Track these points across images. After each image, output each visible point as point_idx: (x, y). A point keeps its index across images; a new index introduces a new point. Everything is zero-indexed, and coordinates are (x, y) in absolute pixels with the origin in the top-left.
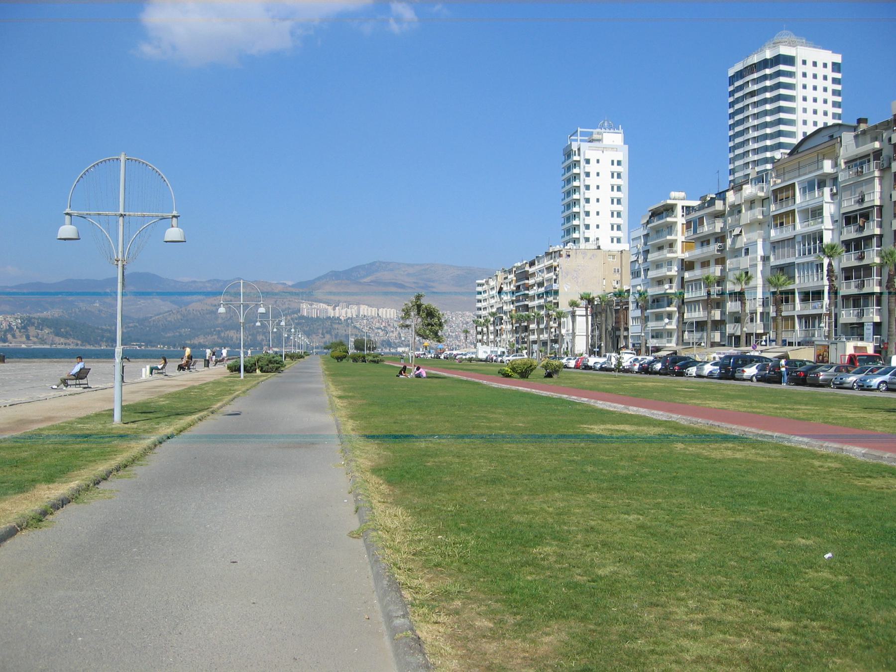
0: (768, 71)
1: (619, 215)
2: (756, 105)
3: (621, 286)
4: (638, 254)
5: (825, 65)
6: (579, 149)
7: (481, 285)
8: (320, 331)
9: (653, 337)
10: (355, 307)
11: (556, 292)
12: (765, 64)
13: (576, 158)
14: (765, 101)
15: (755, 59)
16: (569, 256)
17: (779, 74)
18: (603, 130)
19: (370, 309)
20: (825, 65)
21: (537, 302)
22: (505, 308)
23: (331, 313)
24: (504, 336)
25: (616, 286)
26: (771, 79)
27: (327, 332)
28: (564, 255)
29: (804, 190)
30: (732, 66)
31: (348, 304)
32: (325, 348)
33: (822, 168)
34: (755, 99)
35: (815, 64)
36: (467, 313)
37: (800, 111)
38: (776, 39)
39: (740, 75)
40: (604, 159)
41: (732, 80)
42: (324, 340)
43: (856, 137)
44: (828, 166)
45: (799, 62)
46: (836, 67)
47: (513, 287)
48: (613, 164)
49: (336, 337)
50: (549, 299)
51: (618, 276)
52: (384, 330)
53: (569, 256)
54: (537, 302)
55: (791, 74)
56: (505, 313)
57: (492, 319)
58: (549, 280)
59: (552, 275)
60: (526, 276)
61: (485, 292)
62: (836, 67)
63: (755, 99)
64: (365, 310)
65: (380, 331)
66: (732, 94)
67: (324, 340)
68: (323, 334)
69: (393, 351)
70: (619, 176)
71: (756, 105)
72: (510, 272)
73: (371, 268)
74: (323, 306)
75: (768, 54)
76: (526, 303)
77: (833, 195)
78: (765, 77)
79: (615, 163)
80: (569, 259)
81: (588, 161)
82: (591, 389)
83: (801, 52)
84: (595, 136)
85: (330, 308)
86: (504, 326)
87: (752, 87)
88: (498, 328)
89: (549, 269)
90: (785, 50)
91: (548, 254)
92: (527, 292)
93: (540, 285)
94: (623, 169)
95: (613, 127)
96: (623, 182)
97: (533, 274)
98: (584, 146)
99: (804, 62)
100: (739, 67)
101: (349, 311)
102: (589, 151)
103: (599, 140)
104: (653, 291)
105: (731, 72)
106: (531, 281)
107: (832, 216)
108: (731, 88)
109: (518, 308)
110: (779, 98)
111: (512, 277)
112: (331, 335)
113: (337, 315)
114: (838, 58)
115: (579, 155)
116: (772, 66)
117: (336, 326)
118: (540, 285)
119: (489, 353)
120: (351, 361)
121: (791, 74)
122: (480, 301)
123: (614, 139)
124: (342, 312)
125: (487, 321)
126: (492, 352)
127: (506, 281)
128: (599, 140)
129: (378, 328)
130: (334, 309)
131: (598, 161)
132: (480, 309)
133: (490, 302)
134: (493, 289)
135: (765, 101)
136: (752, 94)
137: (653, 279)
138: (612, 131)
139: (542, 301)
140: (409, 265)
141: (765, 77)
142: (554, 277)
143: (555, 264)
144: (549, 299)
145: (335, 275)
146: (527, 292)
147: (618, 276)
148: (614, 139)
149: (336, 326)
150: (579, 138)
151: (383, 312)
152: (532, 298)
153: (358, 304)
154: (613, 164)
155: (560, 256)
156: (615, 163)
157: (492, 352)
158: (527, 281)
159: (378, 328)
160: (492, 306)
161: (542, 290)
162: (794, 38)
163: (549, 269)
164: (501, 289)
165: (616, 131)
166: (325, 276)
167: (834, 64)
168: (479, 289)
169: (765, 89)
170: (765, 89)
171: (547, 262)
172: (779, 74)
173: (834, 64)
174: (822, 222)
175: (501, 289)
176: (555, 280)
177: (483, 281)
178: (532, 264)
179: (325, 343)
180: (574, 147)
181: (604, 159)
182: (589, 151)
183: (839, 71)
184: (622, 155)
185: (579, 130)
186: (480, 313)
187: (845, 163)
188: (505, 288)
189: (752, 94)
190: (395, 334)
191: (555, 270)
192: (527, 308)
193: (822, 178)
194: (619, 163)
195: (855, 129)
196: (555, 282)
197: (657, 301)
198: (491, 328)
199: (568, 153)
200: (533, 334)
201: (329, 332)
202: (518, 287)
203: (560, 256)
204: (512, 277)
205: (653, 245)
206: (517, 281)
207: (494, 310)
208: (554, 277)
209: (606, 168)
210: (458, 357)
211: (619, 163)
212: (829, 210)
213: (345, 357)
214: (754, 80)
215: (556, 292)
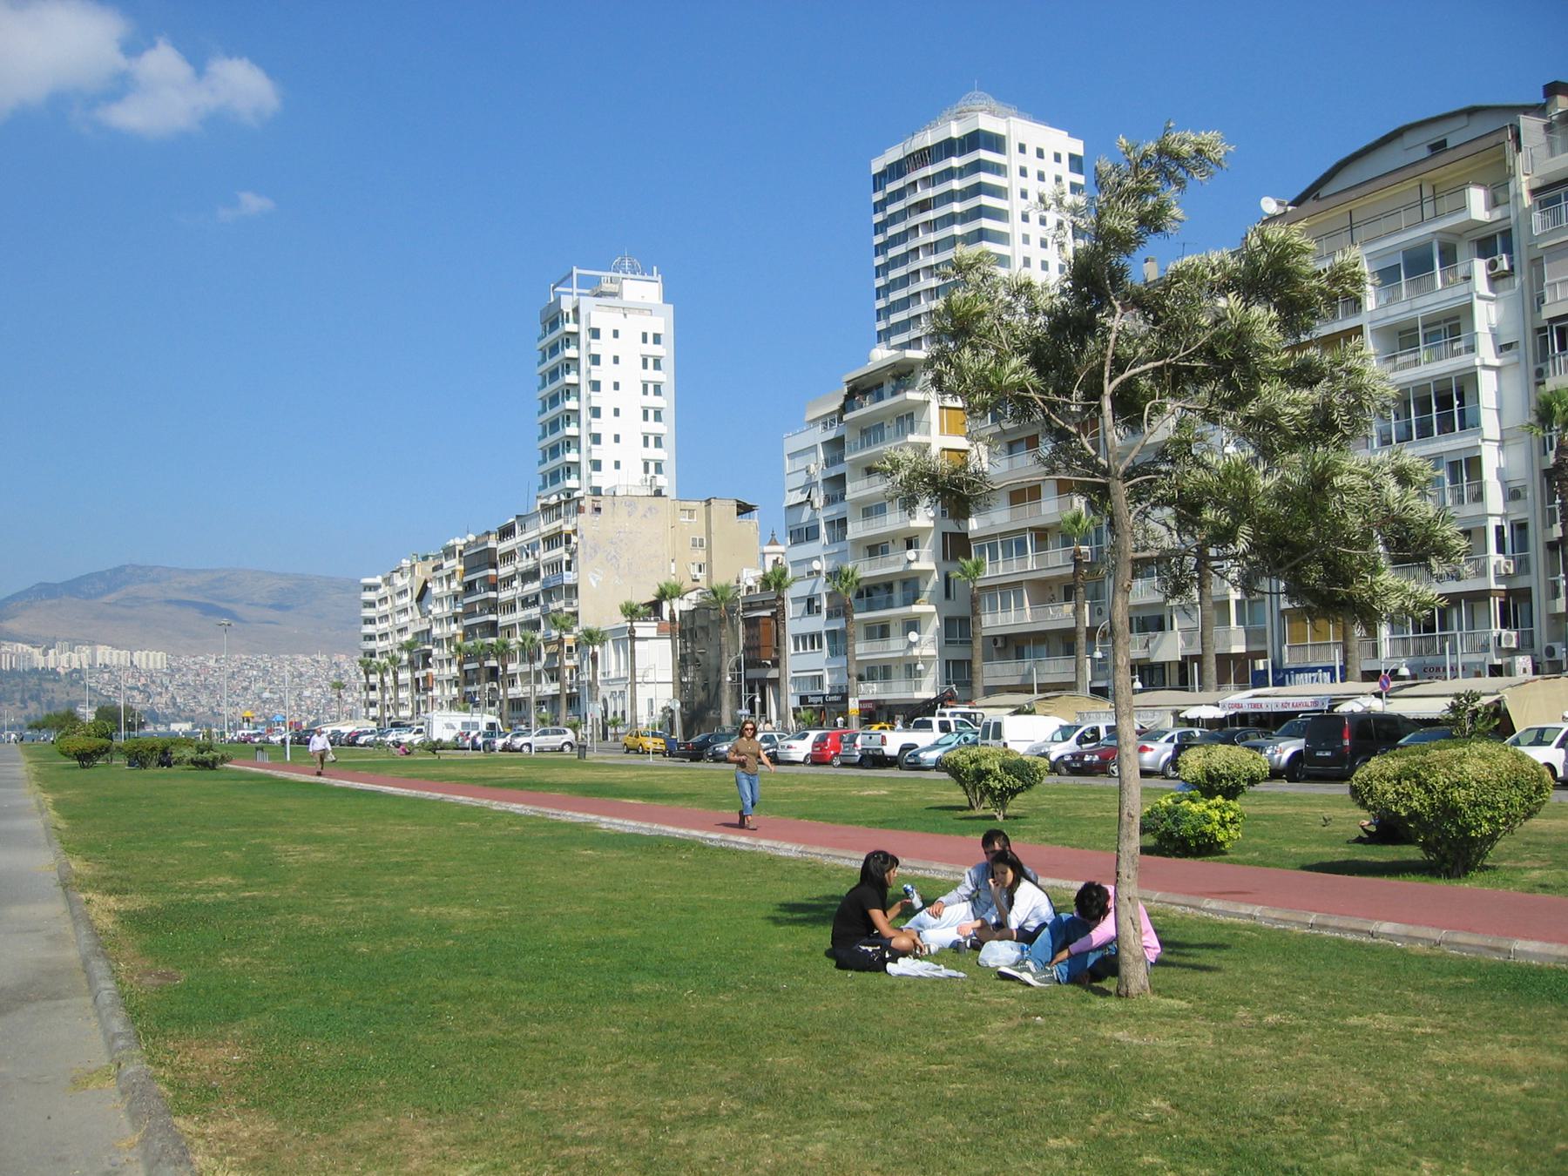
0: (955, 162)
1: (658, 442)
2: (931, 226)
3: (710, 577)
4: (808, 486)
5: (1057, 158)
6: (576, 310)
7: (375, 588)
8: (18, 696)
9: (861, 678)
10: (87, 650)
11: (573, 590)
12: (949, 147)
13: (570, 327)
14: (951, 219)
15: (928, 138)
16: (598, 510)
17: (978, 166)
18: (621, 275)
19: (115, 652)
20: (1057, 158)
21: (520, 615)
22: (436, 631)
23: (39, 660)
24: (436, 692)
25: (699, 576)
26: (961, 177)
27: (31, 698)
28: (589, 509)
29: (1388, 276)
30: (880, 152)
31: (73, 644)
32: (30, 728)
33: (1463, 207)
34: (931, 215)
35: (1040, 153)
36: (301, 658)
37: (1017, 239)
38: (961, 105)
39: (896, 170)
40: (627, 329)
41: (880, 180)
42: (26, 712)
43: (1549, 128)
44: (1477, 205)
45: (1012, 147)
46: (1076, 163)
47: (455, 586)
48: (645, 340)
49: (49, 708)
50: (554, 606)
51: (700, 555)
52: (144, 691)
53: (598, 510)
54: (520, 615)
55: (998, 169)
56: (438, 642)
57: (405, 656)
58: (555, 565)
59: (560, 552)
60: (487, 559)
61: (384, 600)
62: (1076, 163)
63: (931, 215)
64: (105, 654)
65: (135, 693)
66: (880, 206)
67: (26, 712)
68: (23, 701)
69: (162, 729)
70: (657, 366)
71: (931, 226)
72: (449, 552)
73: (114, 579)
74: (22, 647)
75: (956, 130)
76: (492, 617)
77: (1495, 279)
78: (950, 174)
79: (650, 338)
80: (598, 518)
81: (595, 333)
82: (882, 822)
83: (1015, 128)
84: (607, 287)
85: (37, 653)
86: (434, 671)
87: (923, 194)
88: (420, 674)
89: (552, 540)
90: (988, 123)
91: (546, 508)
92: (492, 594)
93: (530, 575)
94: (665, 351)
95: (642, 269)
96: (665, 376)
97: (509, 556)
98: (588, 304)
99: (1022, 149)
100: (894, 154)
101: (75, 656)
102: (597, 314)
103: (613, 295)
104: (868, 570)
105: (877, 166)
106: (504, 571)
107: (1495, 335)
108: (878, 197)
109: (469, 632)
110: (979, 212)
111: (454, 564)
112: (40, 703)
113: (51, 665)
114: (1078, 147)
115: (577, 321)
116: (962, 153)
117: (49, 686)
118: (530, 575)
119: (459, 728)
120: (121, 762)
121: (998, 169)
122: (371, 621)
123: (644, 291)
124: (60, 659)
125: (394, 660)
126: (465, 725)
127: (439, 574)
128: (613, 295)
129: (131, 688)
130: (45, 654)
131: (616, 334)
132: (371, 637)
133: (395, 622)
134: (403, 592)
135: (951, 219)
136: (923, 206)
137: (856, 542)
138: (638, 276)
139: (535, 612)
140: (188, 571)
141: (950, 174)
142: (567, 557)
143: (568, 528)
144: (554, 606)
145: (46, 591)
146: (492, 594)
147: (700, 555)
148: (644, 291)
149: (49, 686)
150: (576, 290)
151: (140, 658)
152: (510, 607)
153: (92, 643)
154: (645, 340)
155: (580, 510)
156: (650, 338)
157: (465, 725)
158: (492, 572)
159: (131, 688)
160: (402, 630)
161: (534, 587)
162: (994, 105)
163: (552, 540)
164: (425, 589)
165: (646, 277)
166: (26, 593)
167: (1072, 157)
168: (369, 596)
169: (950, 196)
170: (950, 196)
171: (545, 527)
172: (978, 166)
173: (1072, 157)
174: (1471, 349)
175: (425, 589)
176: (569, 563)
177: (379, 580)
178: (506, 532)
179: (28, 718)
180: (567, 306)
181: (627, 329)
182: (597, 314)
183: (1080, 172)
184: (662, 321)
185: (576, 271)
186: (371, 645)
187: (1534, 192)
188: (435, 589)
189: (923, 206)
190: (166, 698)
191: (568, 541)
192: (493, 628)
193: (1450, 239)
194: (657, 339)
195: (1539, 110)
196: (569, 569)
197: (875, 592)
198: (405, 676)
199: (553, 319)
200: (512, 683)
201: (36, 698)
202: (469, 587)
203: (580, 510)
204: (454, 564)
205: (854, 463)
206: (467, 571)
207: (408, 637)
208: (567, 557)
209: (632, 349)
210: (362, 740)
211: (657, 339)
212: (1487, 316)
213: (103, 751)
214: (925, 179)
215: (573, 590)
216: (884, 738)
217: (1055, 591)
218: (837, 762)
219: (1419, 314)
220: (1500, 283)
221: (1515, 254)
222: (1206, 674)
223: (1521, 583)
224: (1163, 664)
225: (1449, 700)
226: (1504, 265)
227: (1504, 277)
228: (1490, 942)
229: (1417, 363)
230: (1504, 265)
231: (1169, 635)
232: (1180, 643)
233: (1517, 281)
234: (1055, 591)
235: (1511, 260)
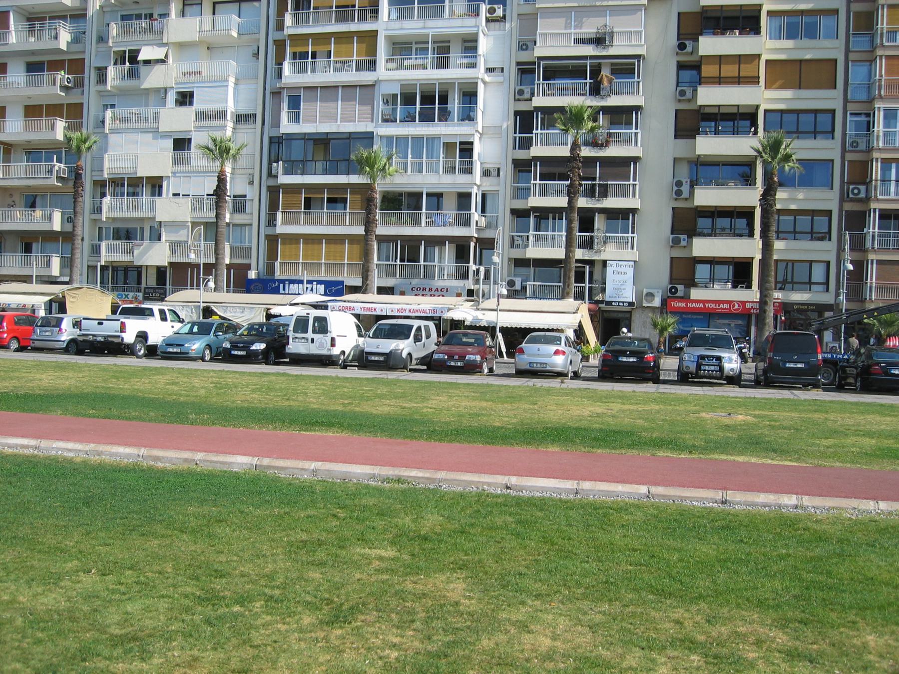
216: (123, 325)
217: (16, 198)
218: (14, 345)
219: (431, 32)
220: (492, 24)
221: (508, 7)
222: (220, 278)
223: (488, 234)
224: (141, 267)
225: (48, 298)
226: (499, 12)
227: (497, 21)
228: (427, 475)
229: (424, 67)
230: (499, 12)
231: (157, 246)
232: (168, 252)
233: (508, 25)
234: (16, 198)
235: (504, 10)
